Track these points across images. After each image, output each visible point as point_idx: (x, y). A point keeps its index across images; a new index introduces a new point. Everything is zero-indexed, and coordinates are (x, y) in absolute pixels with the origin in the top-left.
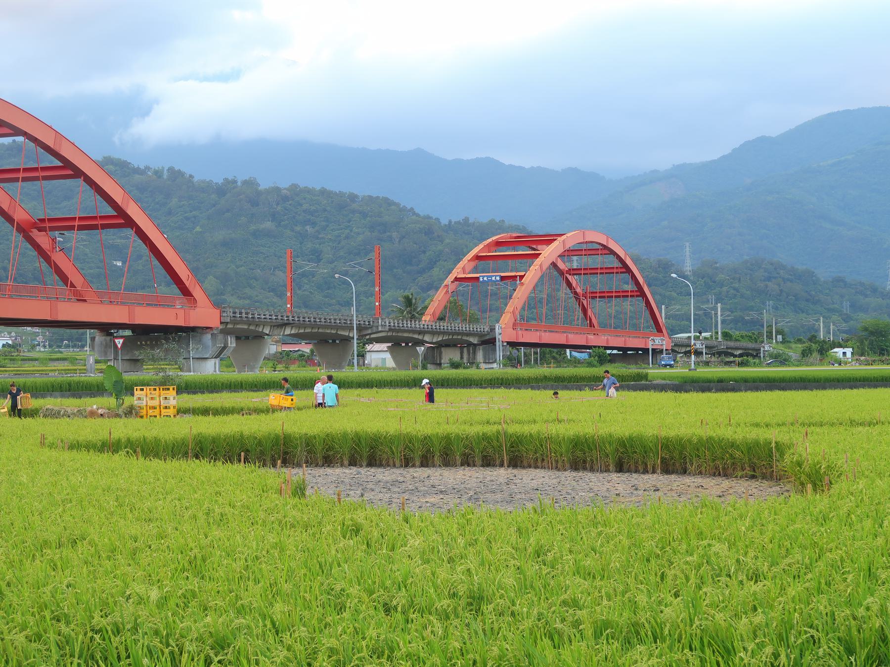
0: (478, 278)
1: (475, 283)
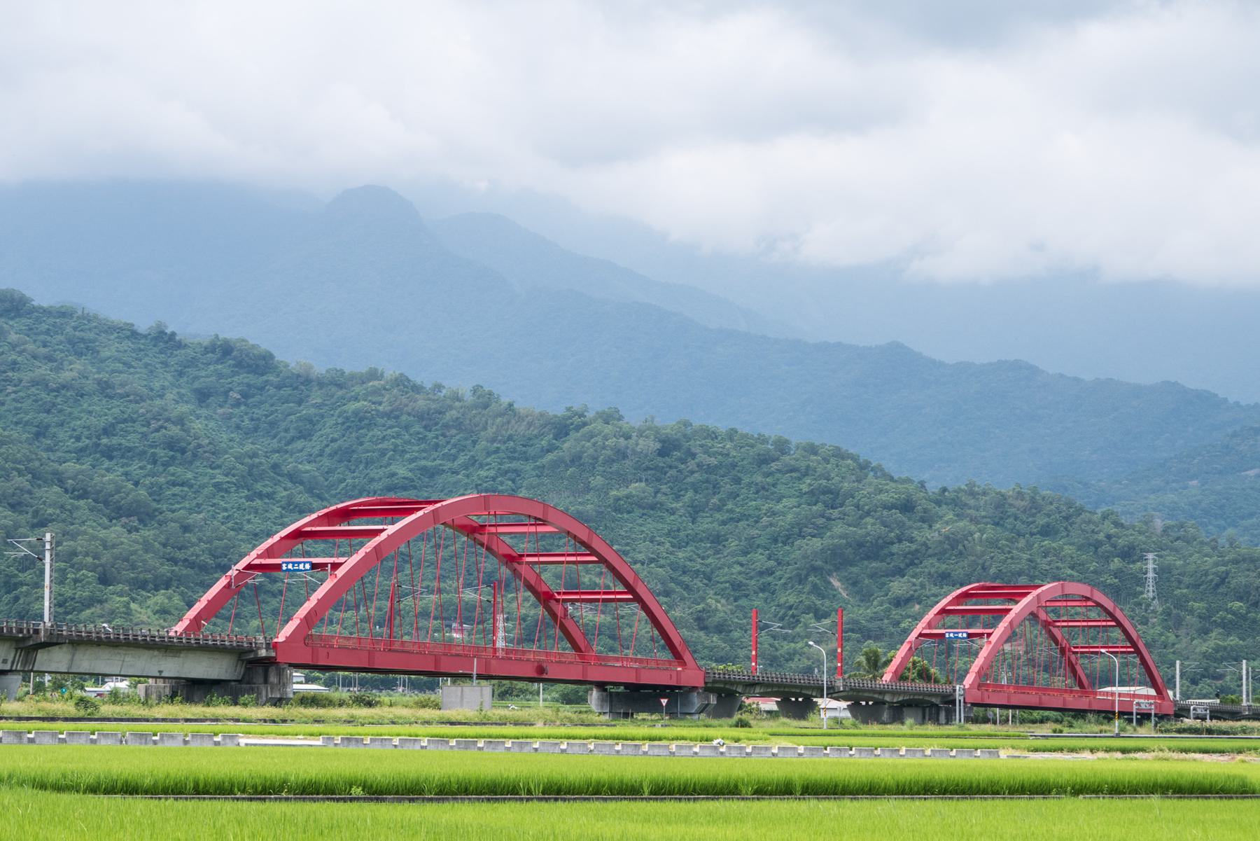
0: (943, 635)
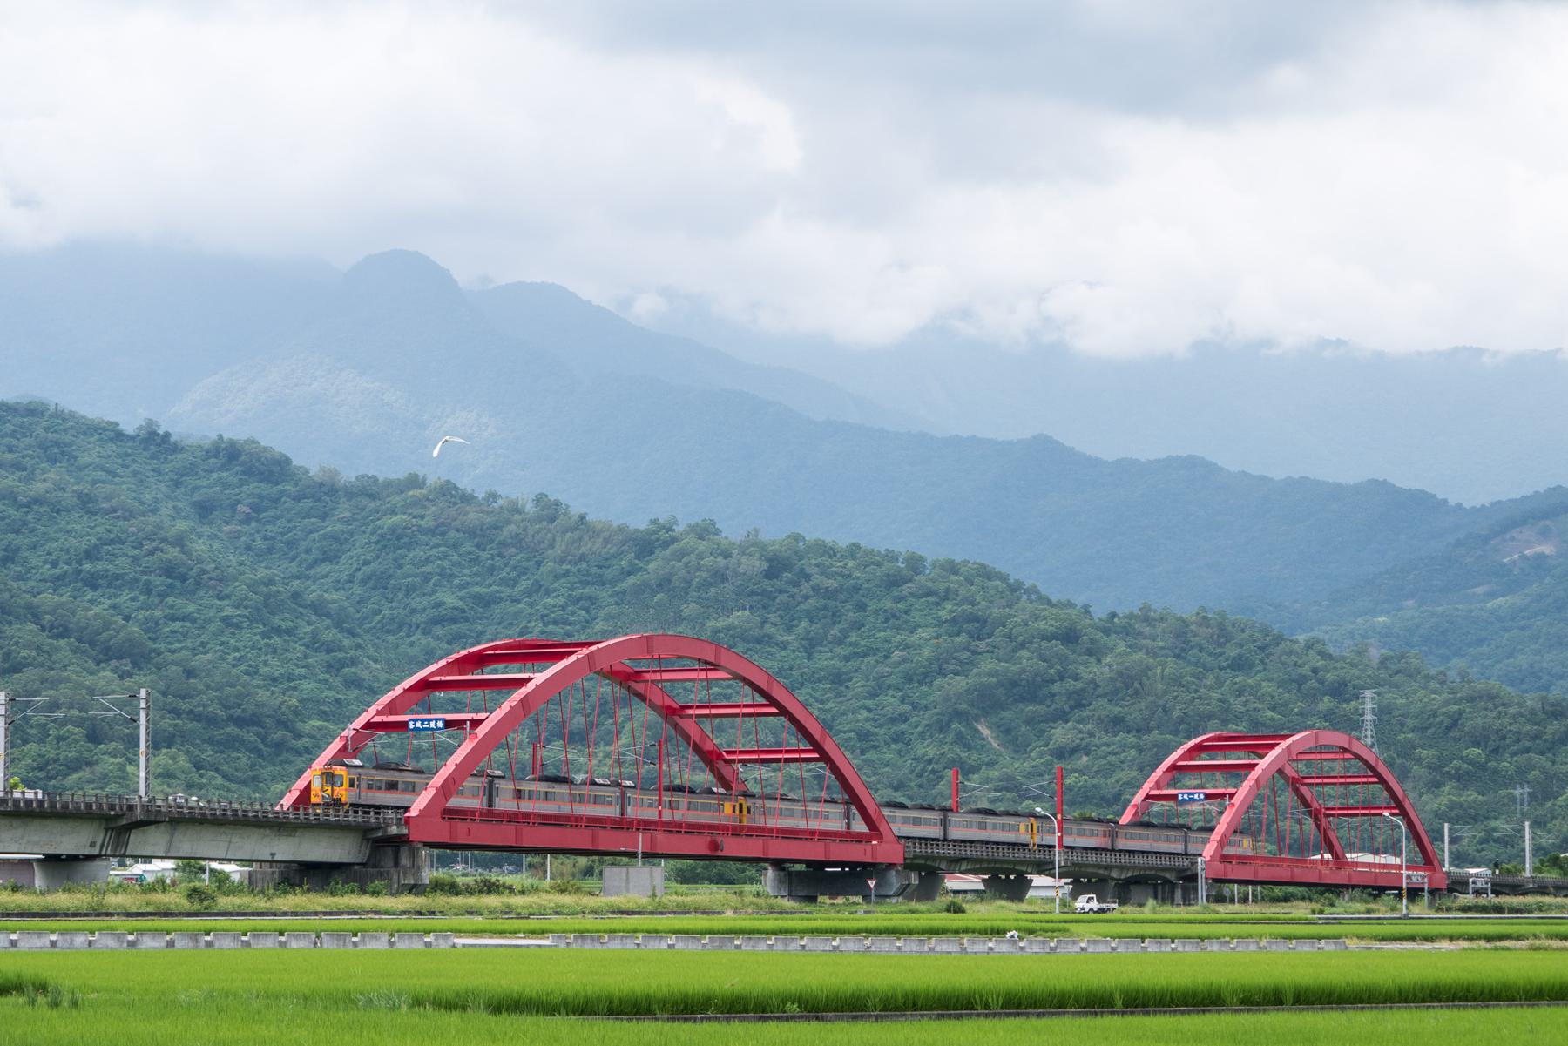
1: (404, 735)
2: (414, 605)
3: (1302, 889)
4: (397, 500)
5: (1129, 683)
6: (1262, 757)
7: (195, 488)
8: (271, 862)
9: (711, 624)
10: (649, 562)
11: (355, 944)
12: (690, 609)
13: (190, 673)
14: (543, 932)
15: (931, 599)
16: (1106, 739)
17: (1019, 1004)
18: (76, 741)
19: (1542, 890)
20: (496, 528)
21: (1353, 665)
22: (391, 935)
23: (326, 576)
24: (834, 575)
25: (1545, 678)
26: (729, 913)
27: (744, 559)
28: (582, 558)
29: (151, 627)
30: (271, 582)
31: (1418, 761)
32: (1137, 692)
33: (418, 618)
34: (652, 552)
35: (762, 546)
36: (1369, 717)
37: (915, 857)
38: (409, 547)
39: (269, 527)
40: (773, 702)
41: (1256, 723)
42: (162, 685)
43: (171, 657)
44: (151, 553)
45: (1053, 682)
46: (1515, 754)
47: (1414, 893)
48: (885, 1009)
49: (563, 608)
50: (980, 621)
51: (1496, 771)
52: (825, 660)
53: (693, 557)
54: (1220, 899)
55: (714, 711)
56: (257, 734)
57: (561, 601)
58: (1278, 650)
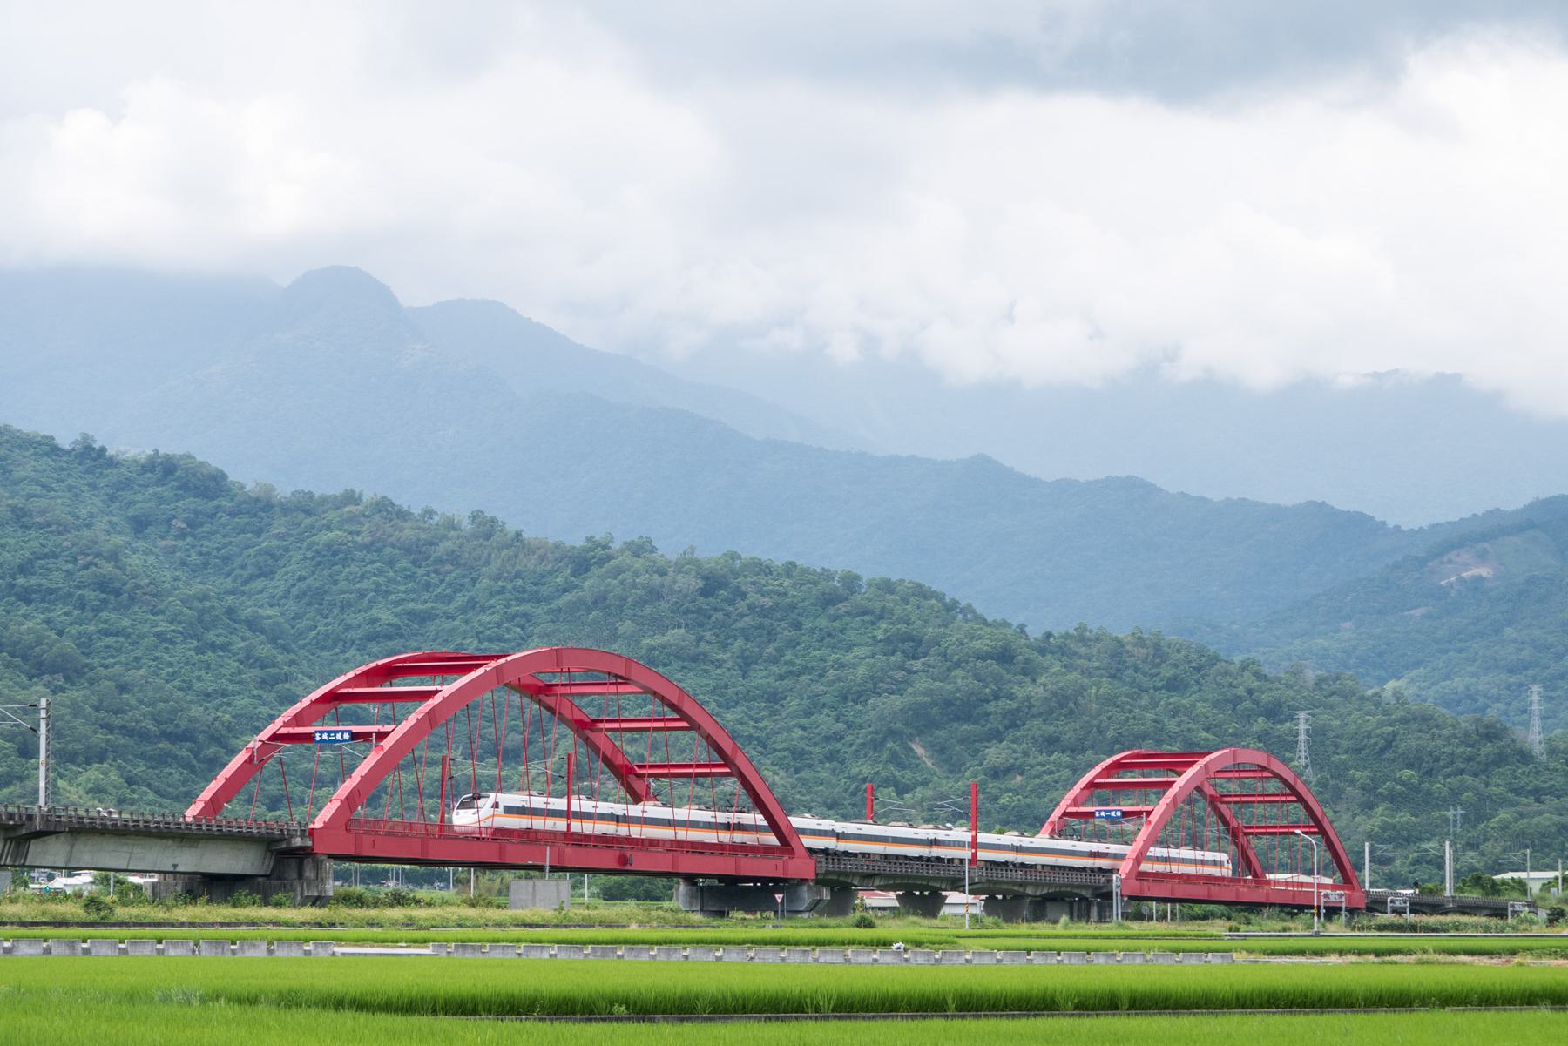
0: (1092, 814)
2: (349, 621)
3: (1222, 907)
4: (331, 515)
5: (1064, 703)
6: (1180, 775)
7: (131, 503)
8: (175, 873)
9: (646, 641)
10: (585, 579)
11: (234, 952)
12: (626, 627)
13: (123, 688)
14: (425, 941)
15: (867, 618)
16: (1040, 759)
17: (850, 1007)
18: (7, 756)
19: (1465, 909)
20: (432, 544)
21: (1288, 686)
22: (271, 943)
23: (261, 592)
24: (769, 594)
25: (1482, 700)
26: (634, 926)
27: (679, 578)
28: (518, 575)
29: (85, 642)
30: (206, 597)
31: (1352, 782)
32: (1071, 712)
33: (352, 635)
34: (587, 570)
35: (697, 563)
36: (1303, 737)
37: (828, 873)
38: (344, 563)
39: (205, 543)
40: (684, 717)
41: (1188, 742)
42: (94, 700)
43: (104, 672)
44: (86, 568)
45: (988, 701)
46: (1449, 776)
47: (1332, 912)
48: (714, 1011)
49: (499, 625)
50: (918, 641)
51: (1429, 793)
52: (760, 679)
53: (628, 576)
54: (1139, 917)
55: (624, 725)
56: (190, 750)
57: (497, 618)
58: (1213, 671)
